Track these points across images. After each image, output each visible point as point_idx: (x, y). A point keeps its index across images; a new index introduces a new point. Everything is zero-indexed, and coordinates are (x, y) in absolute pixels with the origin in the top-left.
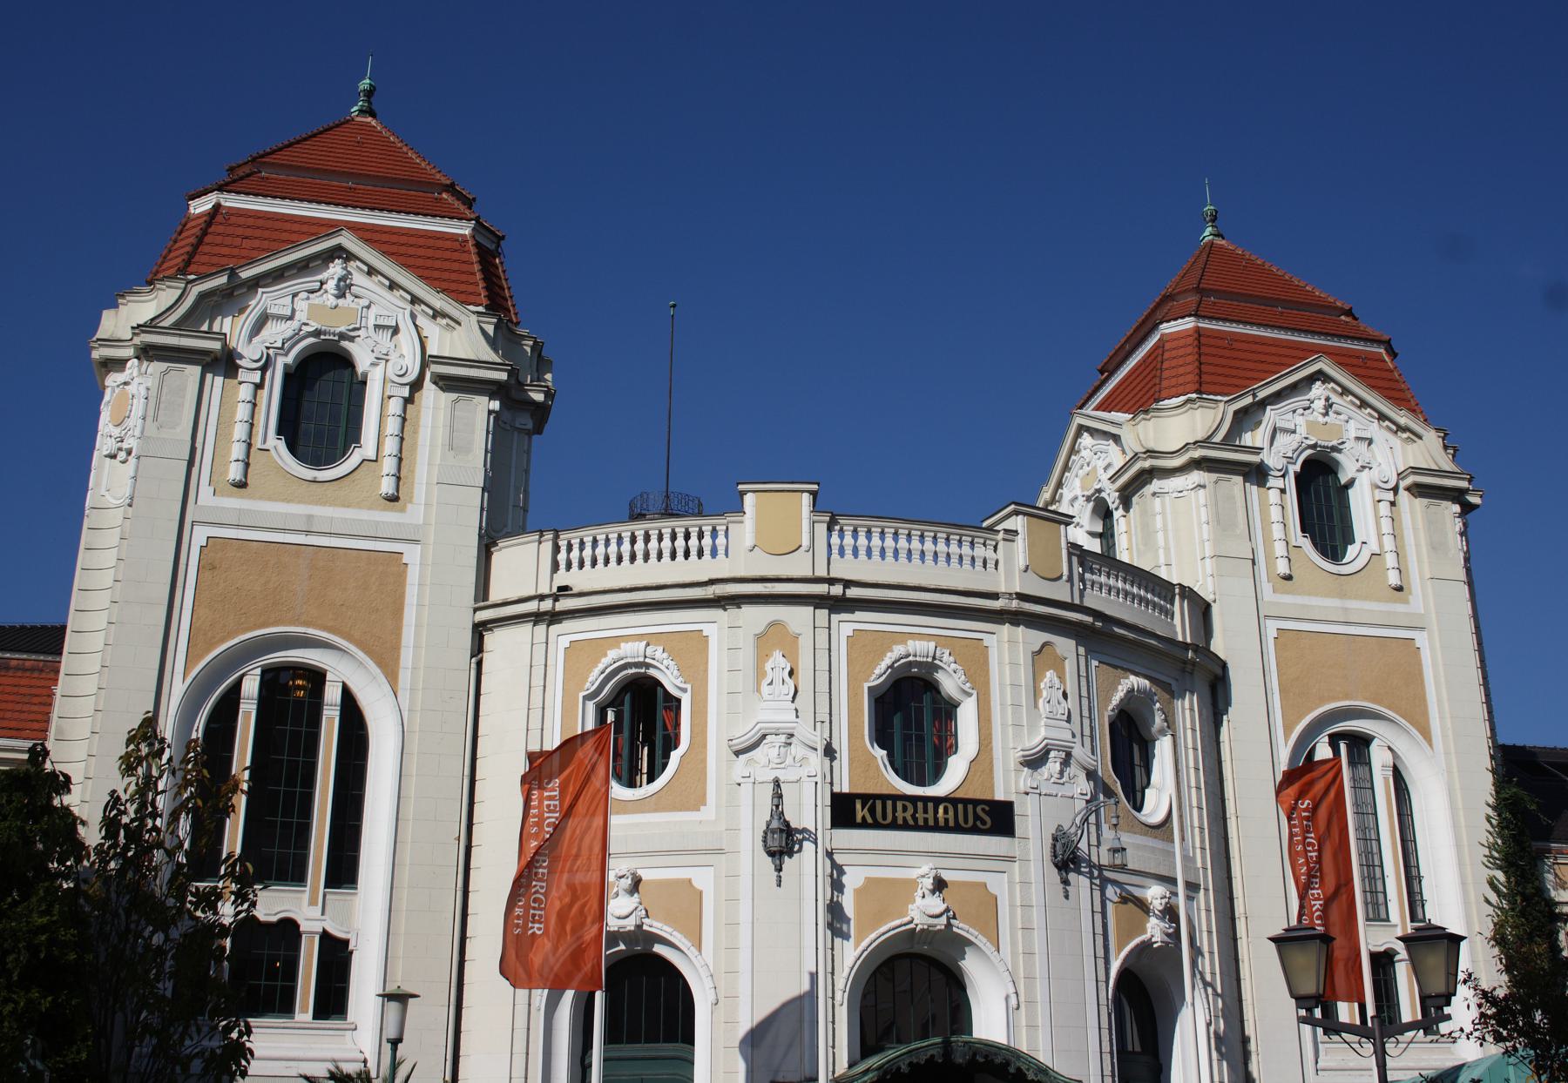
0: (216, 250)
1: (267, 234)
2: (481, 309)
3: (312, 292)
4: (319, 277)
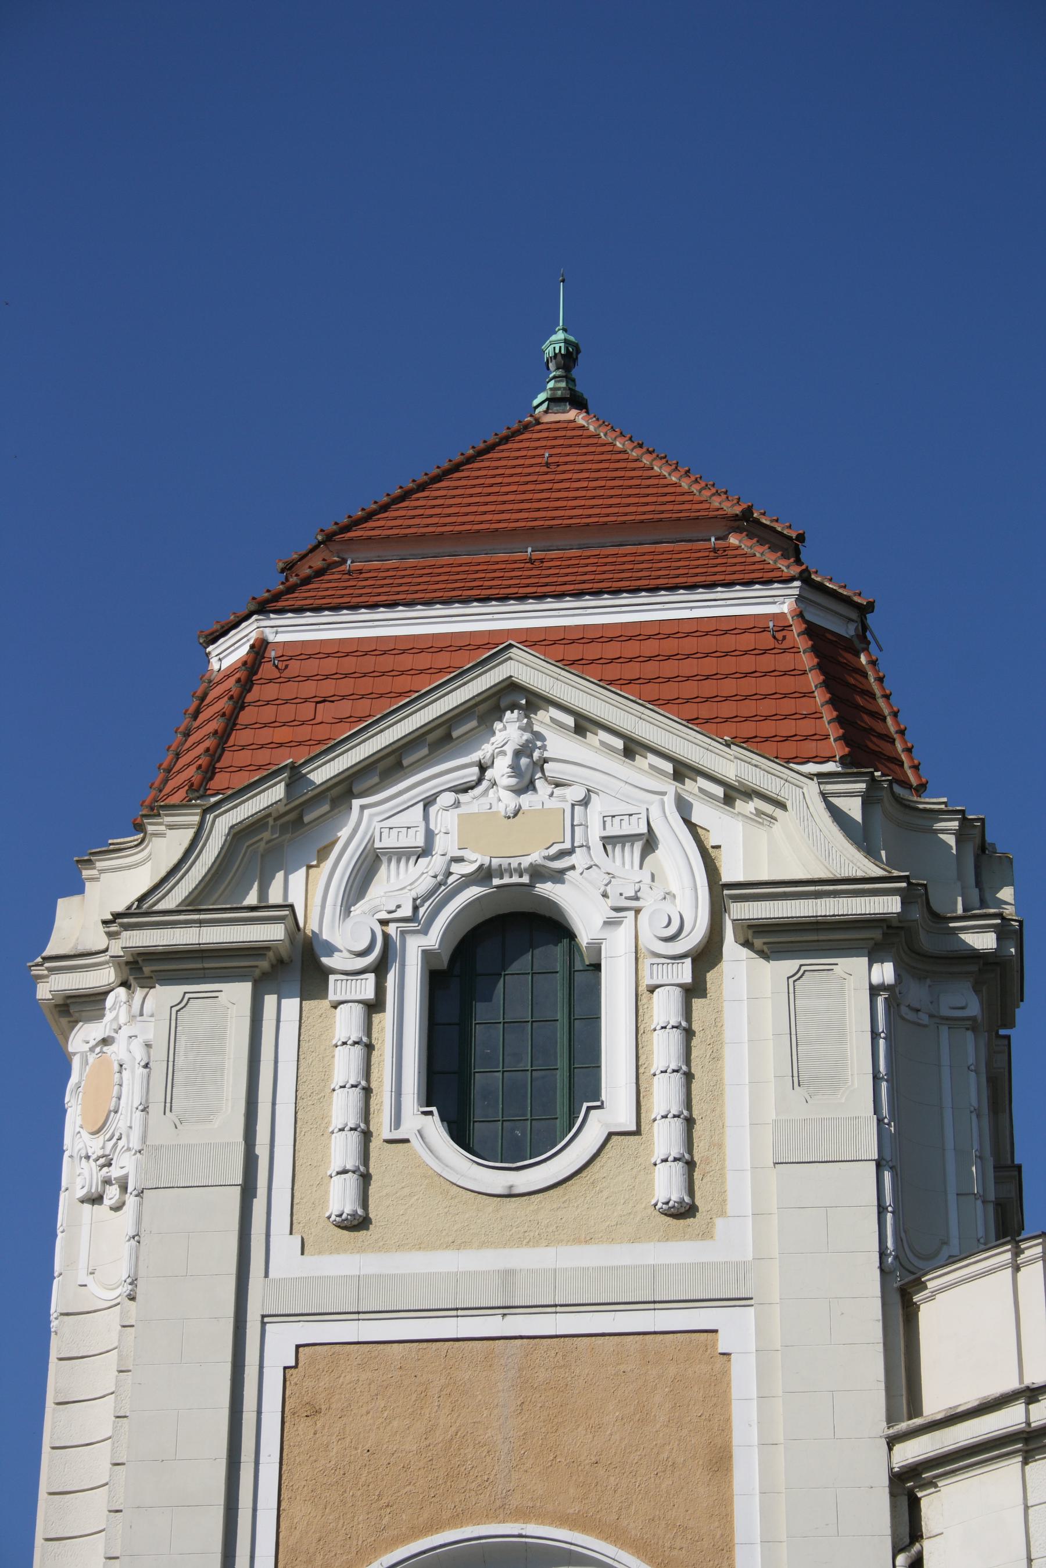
0: (266, 735)
1: (365, 685)
2: (831, 767)
3: (465, 789)
4: (475, 756)
